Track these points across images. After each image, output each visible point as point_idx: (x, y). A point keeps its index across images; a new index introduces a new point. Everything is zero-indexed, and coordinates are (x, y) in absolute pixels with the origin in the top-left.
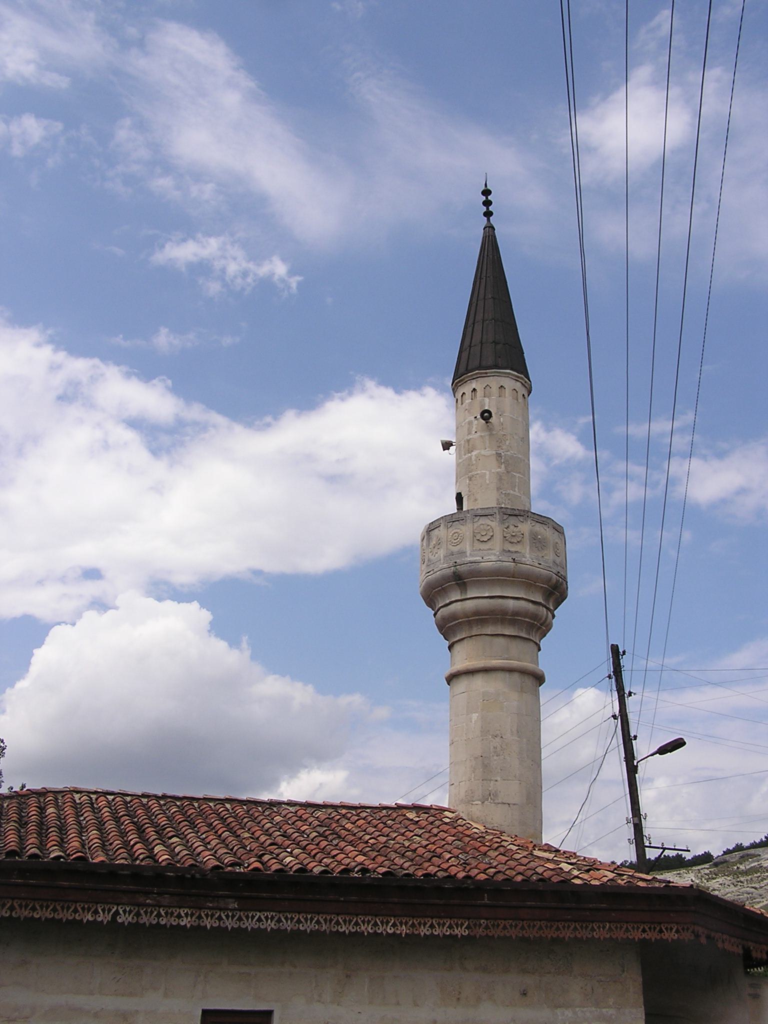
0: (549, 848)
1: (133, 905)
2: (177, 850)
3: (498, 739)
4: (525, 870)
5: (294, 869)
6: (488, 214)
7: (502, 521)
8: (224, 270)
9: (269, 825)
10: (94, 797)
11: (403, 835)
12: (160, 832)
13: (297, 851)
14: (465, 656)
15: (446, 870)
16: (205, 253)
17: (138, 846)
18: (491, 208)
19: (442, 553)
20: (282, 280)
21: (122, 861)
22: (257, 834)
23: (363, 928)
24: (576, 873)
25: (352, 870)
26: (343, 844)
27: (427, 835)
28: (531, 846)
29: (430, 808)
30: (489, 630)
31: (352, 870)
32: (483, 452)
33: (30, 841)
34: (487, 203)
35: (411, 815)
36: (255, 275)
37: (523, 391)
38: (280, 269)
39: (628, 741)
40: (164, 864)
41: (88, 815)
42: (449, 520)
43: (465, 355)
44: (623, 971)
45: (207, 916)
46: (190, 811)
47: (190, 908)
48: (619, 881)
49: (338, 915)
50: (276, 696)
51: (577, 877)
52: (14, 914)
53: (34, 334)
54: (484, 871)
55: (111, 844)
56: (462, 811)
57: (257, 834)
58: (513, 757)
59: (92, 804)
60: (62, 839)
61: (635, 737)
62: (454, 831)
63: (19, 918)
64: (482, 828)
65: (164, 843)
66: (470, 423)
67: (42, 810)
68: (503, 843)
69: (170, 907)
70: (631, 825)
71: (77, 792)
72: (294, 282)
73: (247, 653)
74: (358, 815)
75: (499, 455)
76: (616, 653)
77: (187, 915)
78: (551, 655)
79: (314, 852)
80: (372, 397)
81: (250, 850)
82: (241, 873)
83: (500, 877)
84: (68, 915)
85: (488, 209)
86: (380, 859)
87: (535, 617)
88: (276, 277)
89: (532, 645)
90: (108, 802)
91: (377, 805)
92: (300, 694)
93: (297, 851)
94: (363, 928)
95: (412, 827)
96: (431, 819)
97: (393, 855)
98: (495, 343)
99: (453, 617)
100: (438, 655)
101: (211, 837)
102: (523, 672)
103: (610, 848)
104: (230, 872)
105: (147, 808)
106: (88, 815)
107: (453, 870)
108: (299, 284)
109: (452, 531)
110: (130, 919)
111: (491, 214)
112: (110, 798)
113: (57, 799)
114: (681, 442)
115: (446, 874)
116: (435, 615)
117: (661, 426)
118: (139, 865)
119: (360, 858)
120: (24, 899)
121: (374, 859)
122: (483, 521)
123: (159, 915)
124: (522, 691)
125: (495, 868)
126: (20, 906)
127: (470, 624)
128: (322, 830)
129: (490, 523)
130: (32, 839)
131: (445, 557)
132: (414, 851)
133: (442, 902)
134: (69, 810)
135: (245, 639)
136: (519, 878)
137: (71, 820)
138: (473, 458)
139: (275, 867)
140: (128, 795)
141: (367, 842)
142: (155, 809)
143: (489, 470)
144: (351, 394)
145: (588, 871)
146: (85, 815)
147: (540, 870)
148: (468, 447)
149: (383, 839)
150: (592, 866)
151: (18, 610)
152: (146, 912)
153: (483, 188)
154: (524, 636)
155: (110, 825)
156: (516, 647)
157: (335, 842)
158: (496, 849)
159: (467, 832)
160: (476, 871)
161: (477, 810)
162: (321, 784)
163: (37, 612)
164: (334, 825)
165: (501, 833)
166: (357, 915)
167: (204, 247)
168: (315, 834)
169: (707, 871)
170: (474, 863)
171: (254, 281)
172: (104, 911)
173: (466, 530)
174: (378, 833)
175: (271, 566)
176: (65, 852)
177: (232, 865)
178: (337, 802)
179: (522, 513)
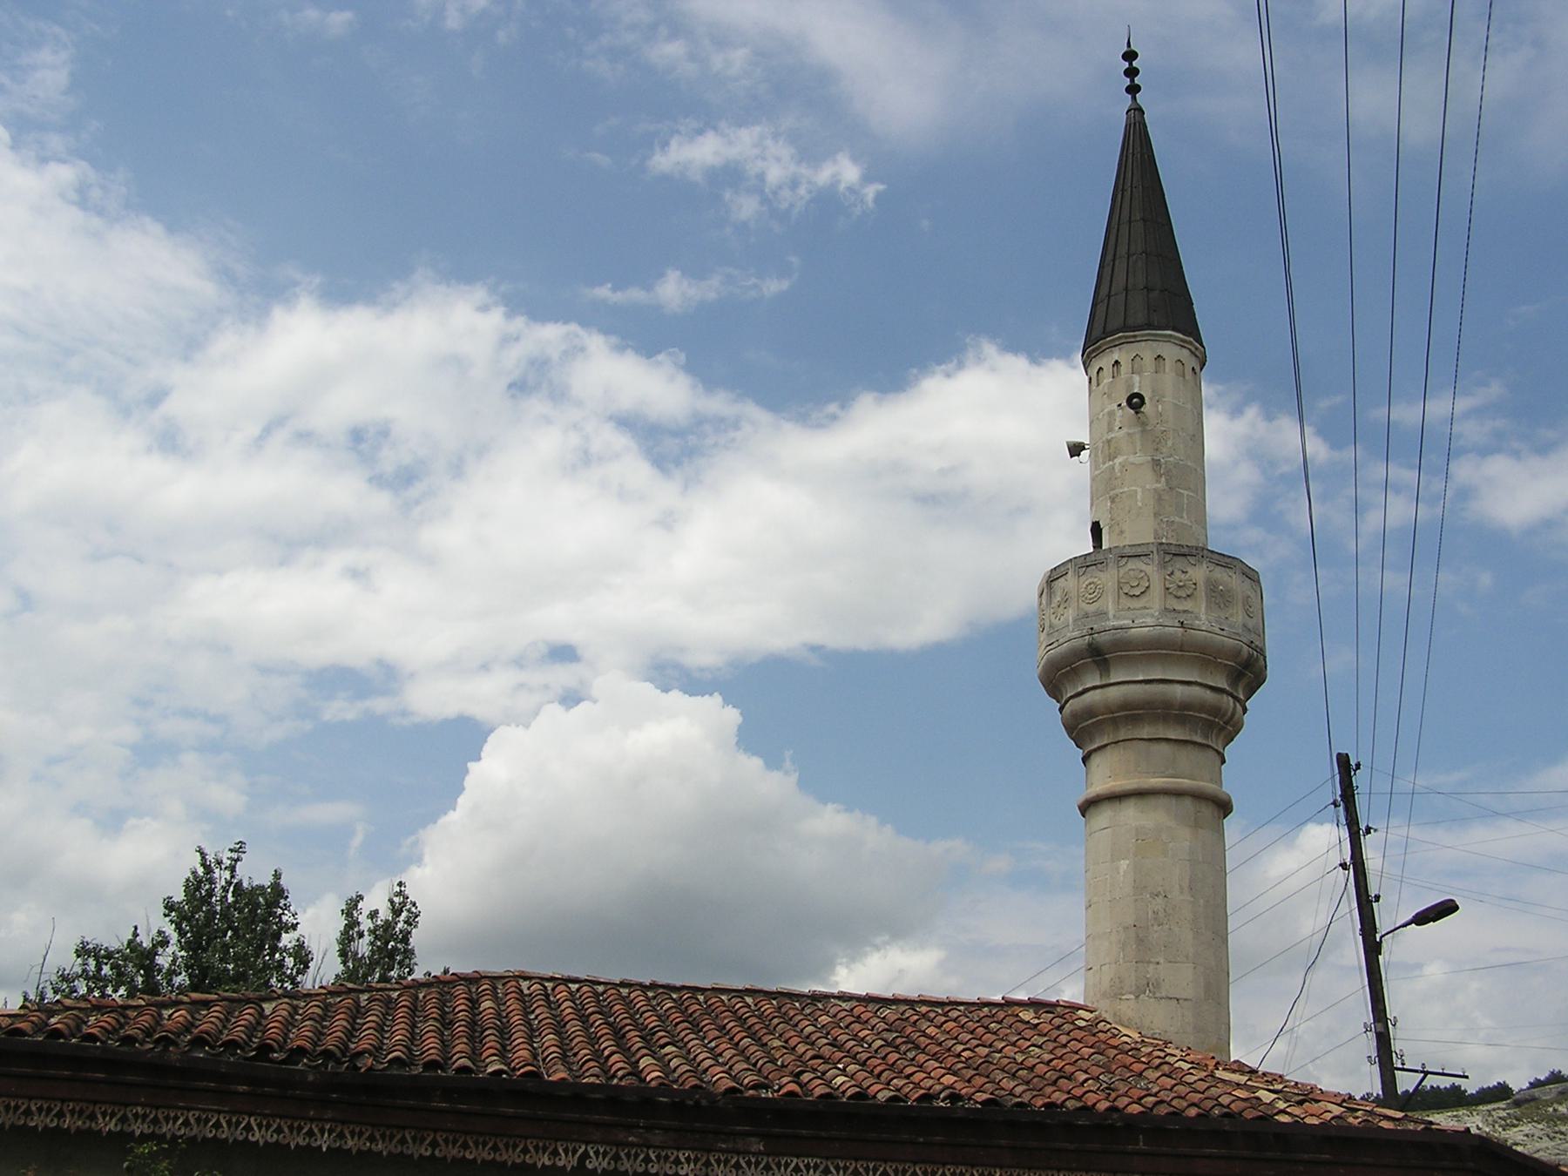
0: (1240, 1068)
1: (608, 1144)
2: (673, 1064)
3: (1160, 900)
4: (1202, 1100)
5: (849, 1093)
6: (1133, 90)
7: (1163, 565)
8: (761, 177)
9: (811, 1029)
10: (549, 985)
11: (1014, 1044)
12: (647, 1037)
13: (852, 1068)
14: (1106, 774)
15: (1079, 1099)
16: (733, 152)
17: (615, 1057)
18: (1137, 80)
19: (1070, 614)
20: (851, 189)
21: (592, 1079)
22: (793, 1042)
24: (1281, 1105)
25: (936, 1097)
26: (922, 1058)
27: (1051, 1045)
28: (1211, 1064)
29: (1057, 1005)
30: (1146, 732)
31: (936, 1097)
32: (1132, 459)
33: (457, 1049)
34: (1131, 73)
35: (1027, 1015)
36: (809, 182)
37: (1191, 362)
38: (848, 172)
39: (1366, 903)
40: (653, 1084)
41: (541, 1012)
42: (1082, 564)
43: (1102, 308)
45: (718, 1162)
46: (692, 1007)
47: (693, 1149)
48: (1351, 1120)
49: (915, 1163)
50: (826, 837)
51: (1283, 1111)
52: (437, 1152)
53: (480, 294)
54: (1139, 1101)
55: (575, 1055)
56: (1105, 1009)
57: (793, 1042)
58: (1190, 926)
59: (547, 996)
60: (504, 1046)
61: (1377, 898)
62: (1093, 1040)
63: (445, 1158)
64: (1136, 1036)
65: (653, 1055)
66: (1111, 414)
67: (474, 1003)
68: (1171, 1060)
69: (663, 1148)
70: (1372, 1035)
71: (526, 978)
72: (870, 192)
73: (794, 777)
74: (945, 1015)
75: (1156, 463)
76: (1345, 766)
77: (688, 1160)
78: (1242, 767)
79: (879, 1069)
80: (993, 369)
81: (783, 1066)
82: (767, 1099)
83: (1163, 1110)
85: (1132, 81)
86: (979, 1081)
87: (1216, 711)
88: (842, 187)
89: (1211, 754)
90: (571, 993)
91: (974, 999)
92: (875, 836)
93: (852, 1068)
95: (1028, 1033)
96: (1058, 1021)
97: (998, 1075)
98: (1148, 289)
99: (1089, 712)
100: (1068, 773)
101: (724, 1046)
102: (1198, 796)
103: (1343, 1073)
104: (752, 1097)
105: (628, 1003)
106: (541, 1012)
107: (1091, 1099)
108: (879, 197)
109: (1085, 581)
110: (605, 1164)
111: (1128, 90)
112: (574, 987)
113: (495, 988)
114: (1471, 431)
115: (1079, 1104)
116: (1061, 709)
117: (1438, 407)
118: (617, 1086)
119: (949, 1079)
120: (451, 1131)
121: (969, 1081)
122: (1133, 564)
124: (1197, 825)
125: (1155, 1095)
126: (446, 1141)
127: (1115, 723)
128: (890, 1036)
129: (1144, 567)
130: (461, 1046)
132: (1032, 1069)
133: (1072, 1147)
134: (513, 1005)
135: (788, 754)
136: (1193, 1112)
137: (516, 1019)
138: (1117, 468)
139: (819, 1091)
140: (600, 983)
141: (959, 1055)
142: (640, 1004)
143: (1141, 487)
144: (961, 366)
145: (1300, 1103)
147: (1225, 1100)
148: (1107, 450)
149: (983, 1051)
150: (1308, 1095)
151: (451, 710)
152: (628, 1155)
153: (1125, 49)
154: (1199, 740)
155: (574, 1027)
156: (1186, 758)
157: (910, 1055)
158: (1157, 1067)
159: (1113, 1042)
160: (1126, 1100)
161: (1128, 1007)
162: (901, 971)
163: (478, 711)
164: (909, 1029)
165: (1166, 1043)
166: (944, 1165)
167: (730, 143)
168: (880, 1042)
169: (1503, 1114)
170: (1123, 1088)
171: (810, 192)
172: (566, 1151)
173: (1107, 578)
174: (975, 1042)
175: (839, 638)
176: (508, 1065)
177: (756, 1087)
178: (914, 995)
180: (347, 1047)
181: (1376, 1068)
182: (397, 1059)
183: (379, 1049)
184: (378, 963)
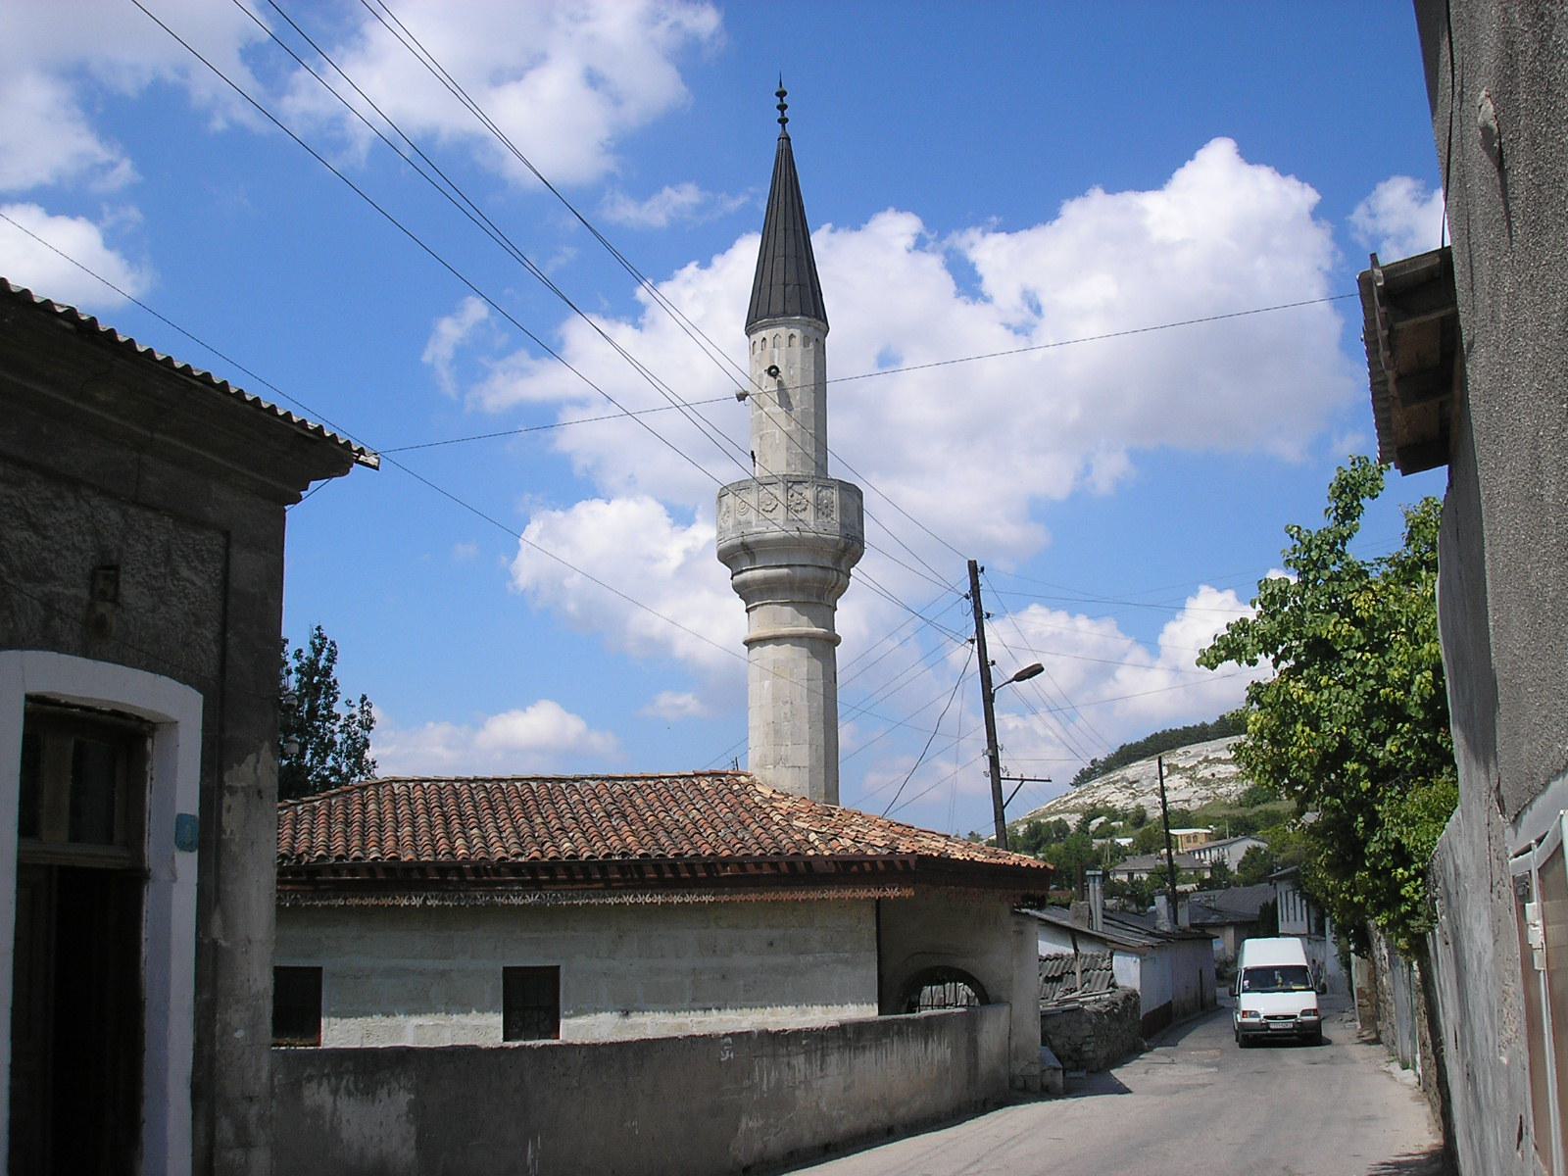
3: (788, 705)
6: (783, 121)
23: (625, 900)
34: (782, 108)
41: (404, 810)
44: (859, 923)
52: (347, 903)
71: (396, 782)
77: (481, 896)
84: (388, 902)
94: (625, 900)
105: (456, 794)
106: (404, 810)
112: (426, 785)
123: (459, 898)
130: (356, 841)
131: (733, 527)
140: (442, 781)
146: (402, 808)
179: (807, 479)
180: (293, 847)
181: (989, 779)
182: (321, 855)
183: (310, 848)
184: (306, 695)
